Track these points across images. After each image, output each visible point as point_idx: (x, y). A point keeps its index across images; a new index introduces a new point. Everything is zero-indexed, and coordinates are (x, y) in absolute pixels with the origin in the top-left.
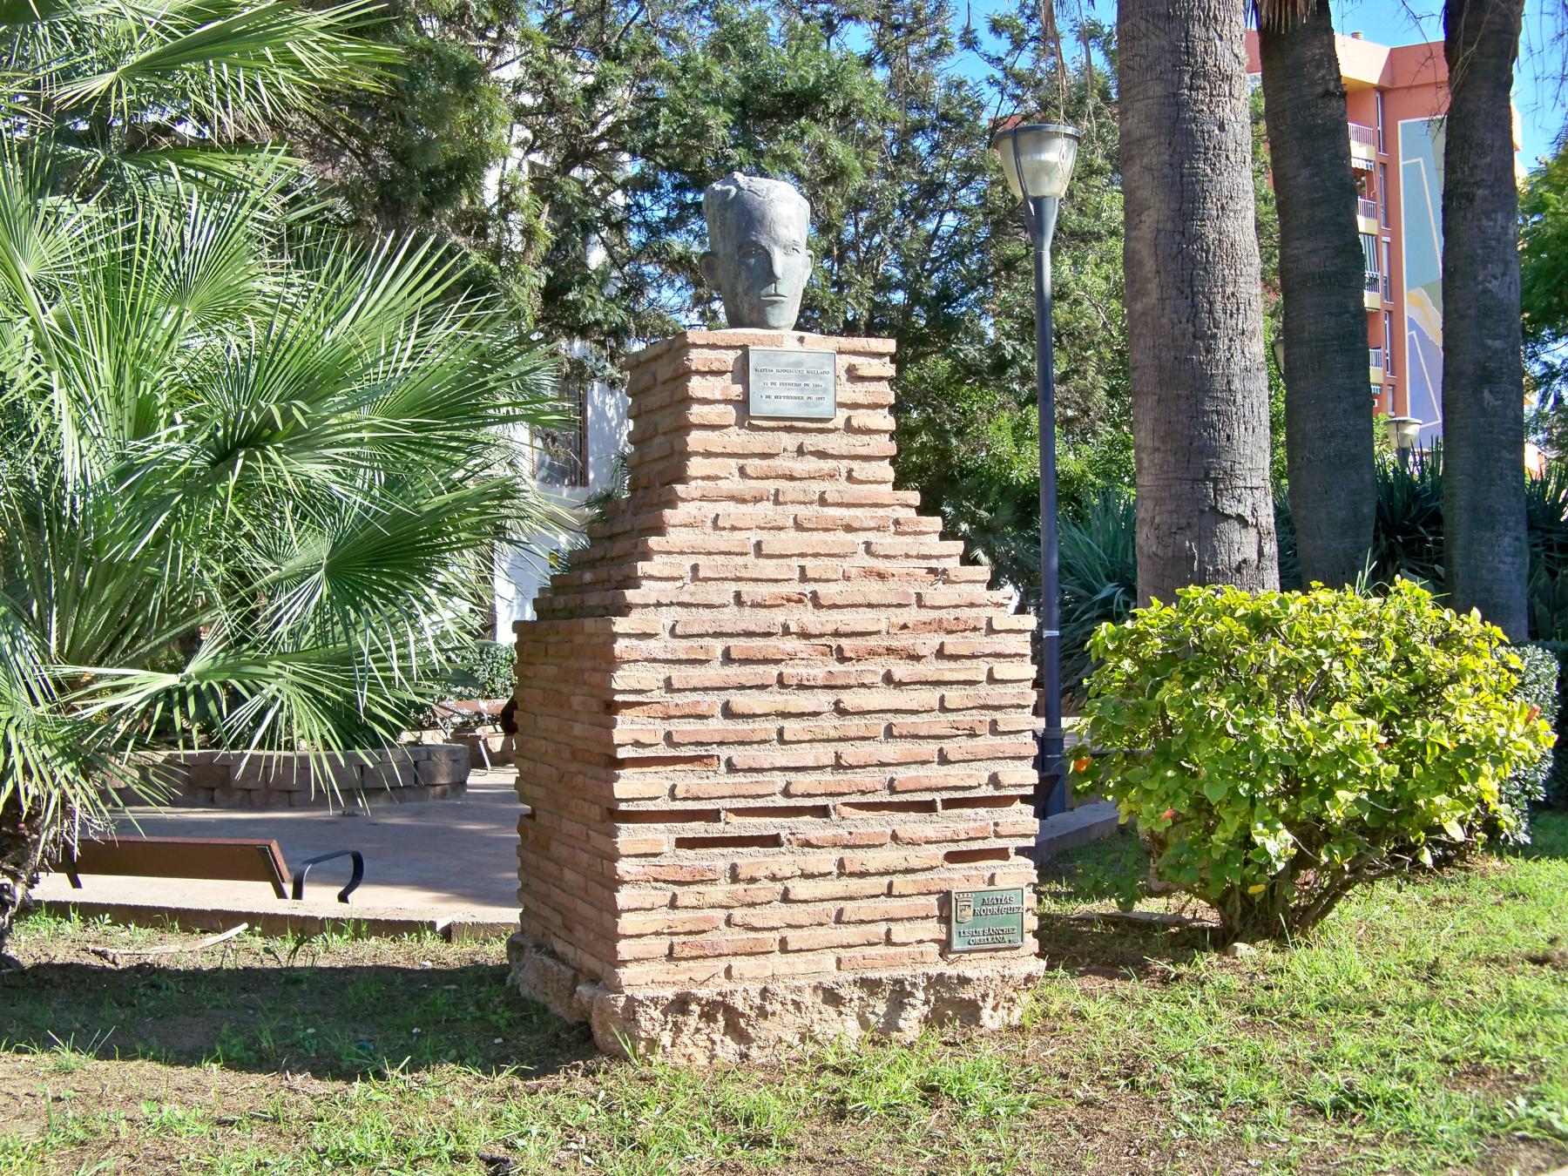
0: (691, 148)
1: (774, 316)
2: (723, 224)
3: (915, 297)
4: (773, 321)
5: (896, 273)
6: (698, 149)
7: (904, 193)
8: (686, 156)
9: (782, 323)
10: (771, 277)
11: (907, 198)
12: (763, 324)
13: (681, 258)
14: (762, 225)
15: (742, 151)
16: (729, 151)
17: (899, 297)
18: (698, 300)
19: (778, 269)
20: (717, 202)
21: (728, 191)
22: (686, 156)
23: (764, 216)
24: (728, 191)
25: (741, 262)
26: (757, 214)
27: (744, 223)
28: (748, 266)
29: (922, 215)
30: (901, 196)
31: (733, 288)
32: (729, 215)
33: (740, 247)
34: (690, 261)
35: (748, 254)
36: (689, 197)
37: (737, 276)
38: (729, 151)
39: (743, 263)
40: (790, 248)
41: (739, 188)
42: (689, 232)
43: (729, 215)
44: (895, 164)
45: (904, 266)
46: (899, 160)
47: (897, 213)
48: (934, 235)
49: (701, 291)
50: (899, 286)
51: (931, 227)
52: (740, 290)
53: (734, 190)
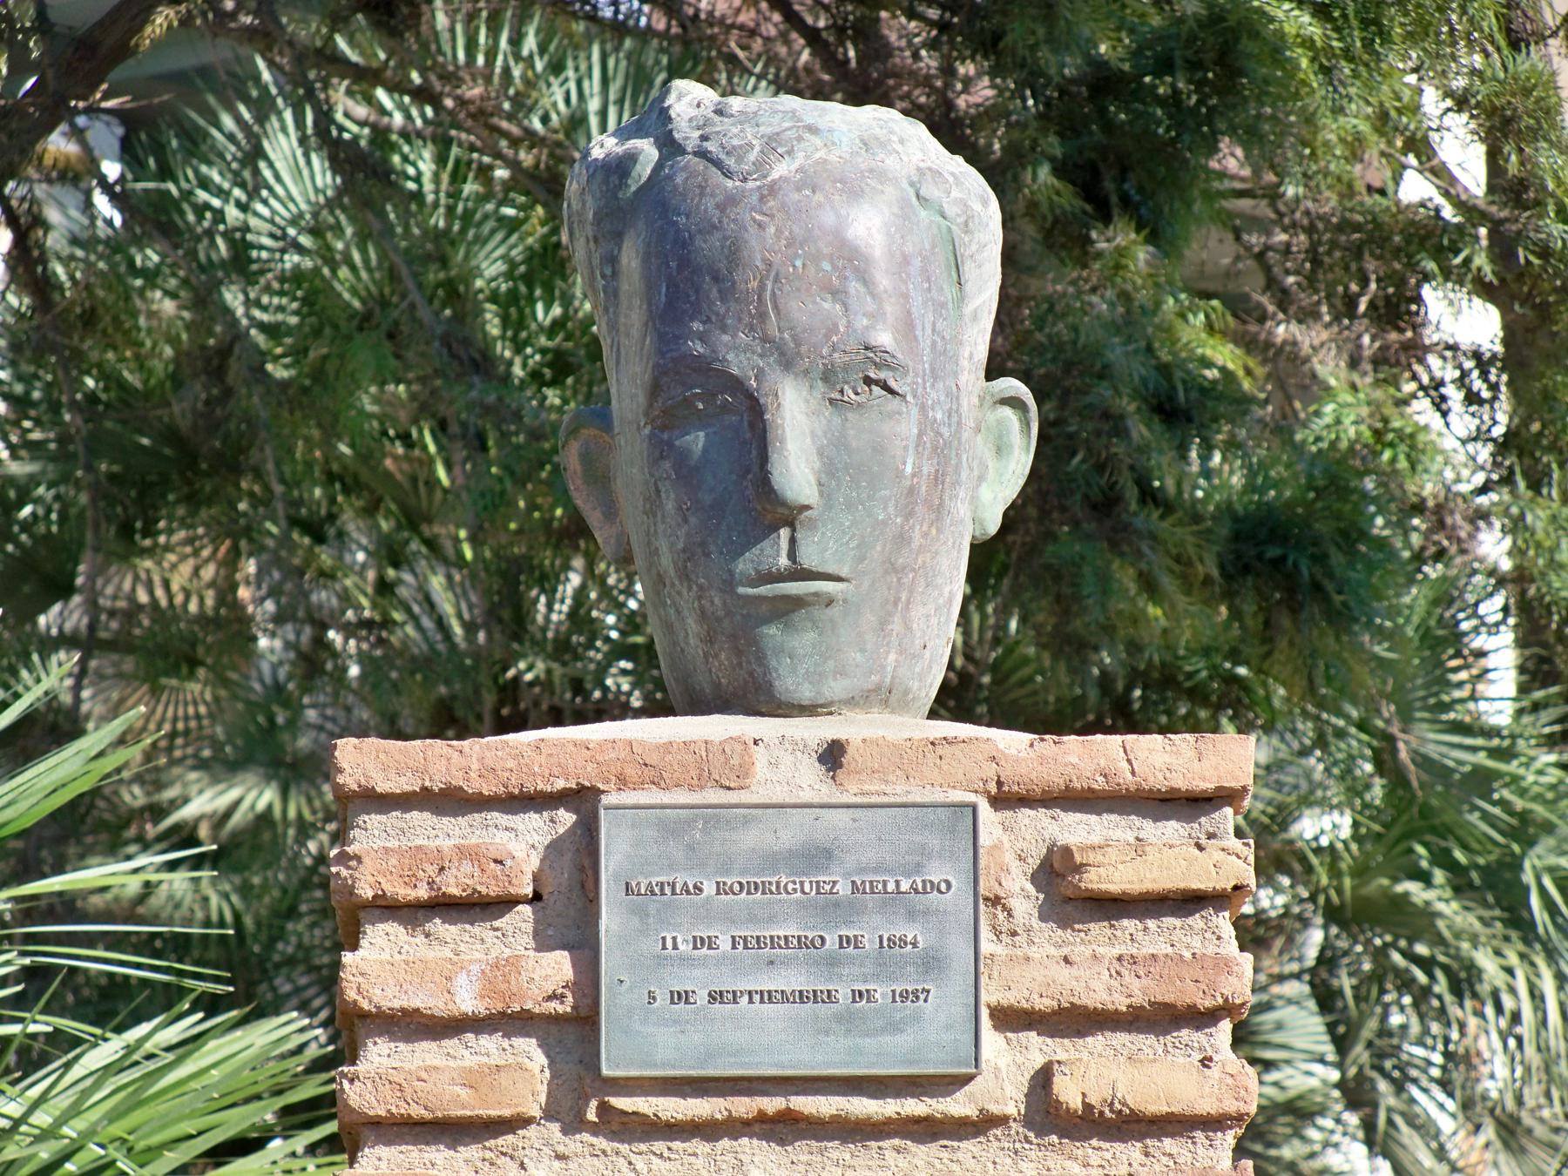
4: (791, 682)
9: (835, 688)
19: (797, 469)
23: (734, 253)
26: (708, 247)
28: (682, 457)
41: (670, 146)
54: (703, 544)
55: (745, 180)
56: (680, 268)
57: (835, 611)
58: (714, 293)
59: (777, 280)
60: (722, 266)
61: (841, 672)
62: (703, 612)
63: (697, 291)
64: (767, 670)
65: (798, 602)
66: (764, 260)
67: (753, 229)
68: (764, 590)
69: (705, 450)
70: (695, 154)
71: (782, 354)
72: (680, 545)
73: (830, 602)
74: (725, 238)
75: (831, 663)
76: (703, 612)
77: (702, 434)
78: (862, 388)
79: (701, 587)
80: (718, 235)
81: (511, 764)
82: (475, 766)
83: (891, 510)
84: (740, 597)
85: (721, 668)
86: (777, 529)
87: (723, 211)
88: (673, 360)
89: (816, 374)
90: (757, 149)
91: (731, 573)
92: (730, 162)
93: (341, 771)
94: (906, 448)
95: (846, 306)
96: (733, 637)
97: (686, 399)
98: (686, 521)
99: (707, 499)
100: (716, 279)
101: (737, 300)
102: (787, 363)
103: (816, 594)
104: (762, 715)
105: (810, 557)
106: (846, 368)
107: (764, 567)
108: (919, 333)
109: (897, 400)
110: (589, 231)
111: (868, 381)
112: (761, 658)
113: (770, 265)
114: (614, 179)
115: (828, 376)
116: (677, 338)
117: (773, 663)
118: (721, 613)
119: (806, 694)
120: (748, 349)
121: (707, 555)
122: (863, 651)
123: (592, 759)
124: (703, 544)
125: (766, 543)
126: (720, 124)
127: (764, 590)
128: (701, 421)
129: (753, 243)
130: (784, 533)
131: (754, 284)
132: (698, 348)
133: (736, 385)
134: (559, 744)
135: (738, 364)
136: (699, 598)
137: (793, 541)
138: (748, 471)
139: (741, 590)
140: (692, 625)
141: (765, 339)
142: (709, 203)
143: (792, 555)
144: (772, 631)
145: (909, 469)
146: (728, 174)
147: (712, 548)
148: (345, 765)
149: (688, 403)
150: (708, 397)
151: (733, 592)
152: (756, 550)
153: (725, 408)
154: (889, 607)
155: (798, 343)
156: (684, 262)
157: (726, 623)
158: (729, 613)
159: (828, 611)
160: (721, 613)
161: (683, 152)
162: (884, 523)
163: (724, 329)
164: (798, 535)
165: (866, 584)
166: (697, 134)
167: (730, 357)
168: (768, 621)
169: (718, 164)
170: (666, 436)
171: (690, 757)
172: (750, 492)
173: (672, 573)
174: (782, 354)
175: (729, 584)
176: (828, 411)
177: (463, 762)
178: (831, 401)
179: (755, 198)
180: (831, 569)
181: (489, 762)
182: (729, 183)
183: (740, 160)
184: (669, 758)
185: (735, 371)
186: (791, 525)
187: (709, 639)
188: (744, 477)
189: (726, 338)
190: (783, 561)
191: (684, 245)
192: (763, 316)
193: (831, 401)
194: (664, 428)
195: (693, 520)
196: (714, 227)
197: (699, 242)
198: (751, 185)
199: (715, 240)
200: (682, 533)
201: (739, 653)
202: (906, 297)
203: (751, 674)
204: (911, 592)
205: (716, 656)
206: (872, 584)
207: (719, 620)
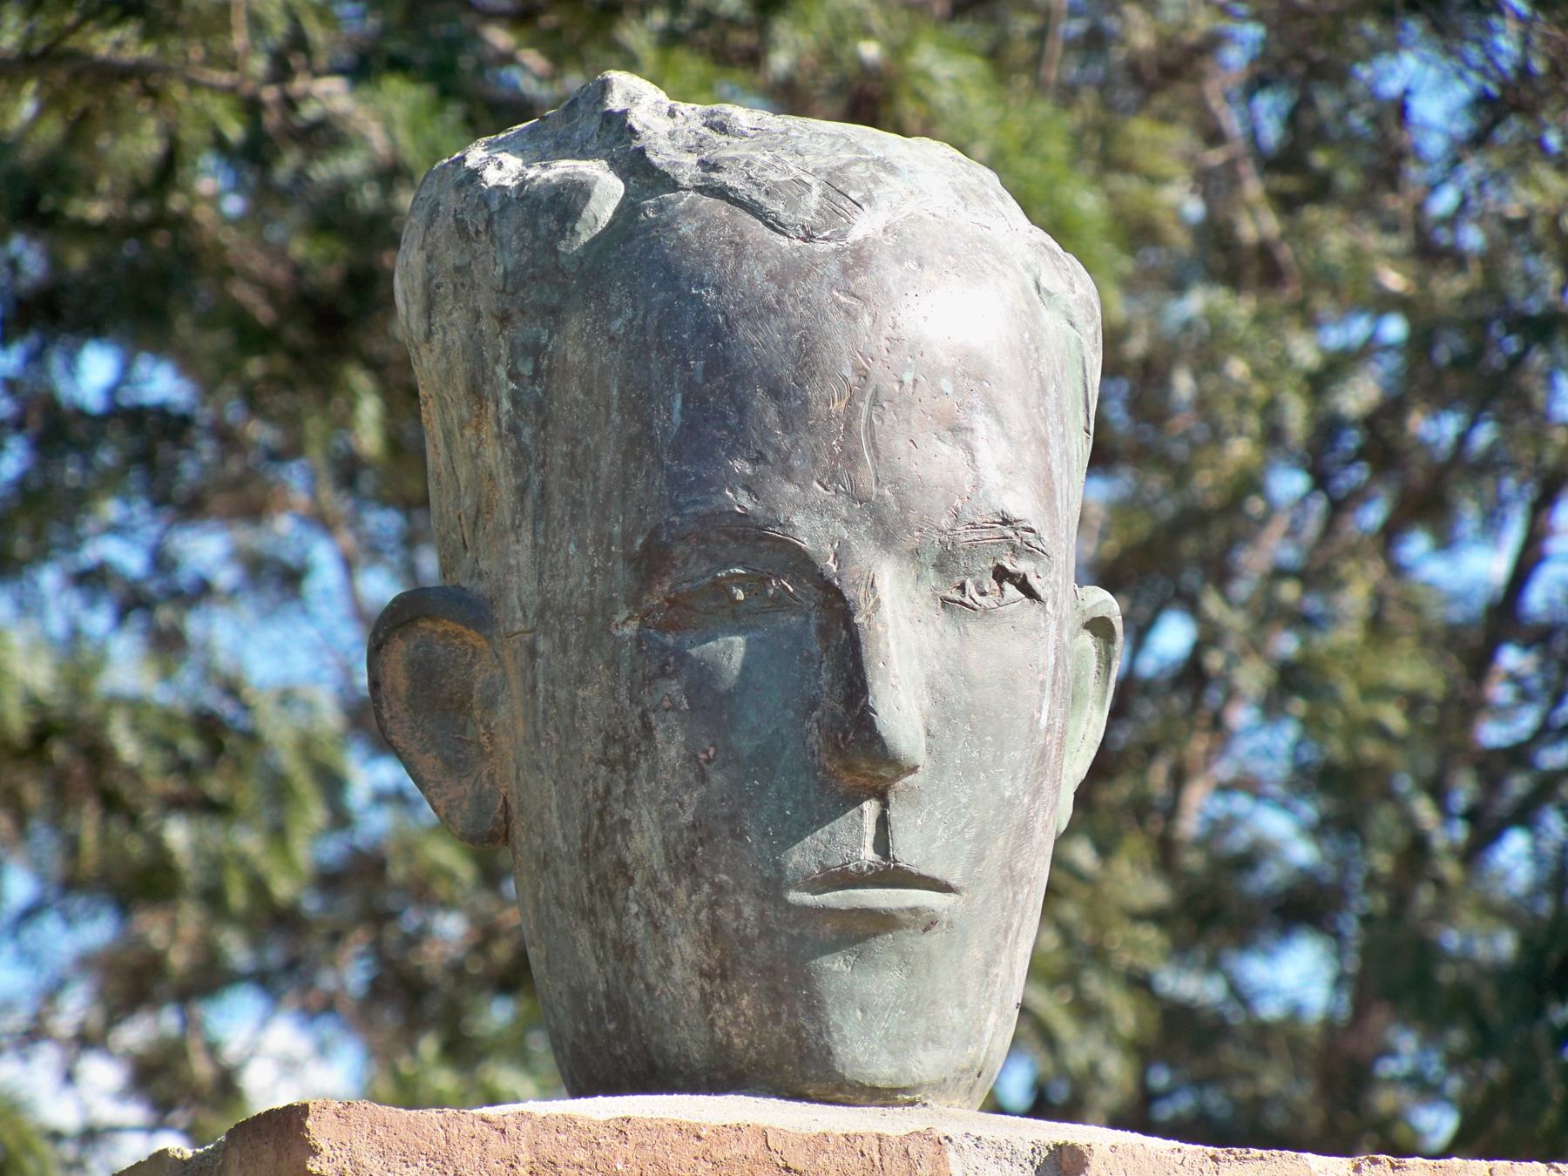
0: (111, 74)
1: (866, 1005)
2: (535, 409)
3: (1396, 973)
4: (860, 1049)
5: (1287, 837)
6: (147, 81)
7: (1336, 367)
8: (78, 130)
9: (925, 1064)
10: (852, 756)
11: (1358, 395)
12: (802, 1071)
13: (43, 732)
14: (795, 414)
15: (402, 96)
16: (329, 94)
17: (1296, 977)
18: (132, 983)
19: (901, 708)
20: (496, 264)
21: (566, 202)
22: (78, 130)
23: (806, 352)
24: (566, 202)
25: (659, 660)
26: (761, 342)
27: (694, 377)
28: (702, 679)
29: (1427, 504)
30: (1320, 382)
31: (602, 832)
32: (573, 343)
33: (650, 561)
34: (97, 753)
35: (706, 609)
36: (93, 373)
37: (626, 750)
38: (329, 94)
39: (672, 663)
40: (980, 568)
41: (638, 169)
42: (92, 580)
43: (573, 343)
44: (1286, 204)
45: (1341, 790)
46: (1295, 174)
47: (1289, 484)
48: (1505, 614)
49: (153, 928)
50: (1303, 908)
51: (1483, 565)
52: (645, 842)
53: (607, 190)
54: (732, 818)
55: (809, 238)
56: (709, 371)
57: (934, 939)
58: (771, 416)
59: (875, 401)
60: (786, 372)
61: (932, 1040)
62: (716, 927)
63: (741, 410)
64: (823, 1030)
65: (884, 921)
66: (857, 369)
67: (837, 319)
68: (833, 898)
69: (745, 668)
70: (699, 189)
71: (879, 521)
72: (687, 818)
73: (930, 924)
74: (790, 329)
75: (922, 1023)
76: (716, 927)
77: (739, 640)
78: (990, 584)
79: (719, 888)
80: (776, 323)
81: (580, 1156)
82: (525, 1157)
83: (1020, 783)
84: (790, 907)
85: (741, 1019)
86: (857, 802)
87: (782, 285)
88: (699, 518)
89: (928, 559)
90: (816, 191)
91: (779, 867)
92: (777, 207)
93: (314, 1152)
94: (1042, 689)
95: (969, 449)
96: (770, 971)
97: (716, 583)
98: (703, 778)
99: (746, 745)
100: (775, 393)
101: (810, 430)
102: (886, 537)
103: (915, 911)
104: (811, 1100)
105: (909, 851)
106: (973, 550)
107: (835, 862)
108: (1058, 503)
109: (1033, 608)
110: (485, 300)
111: (1001, 574)
112: (814, 1007)
113: (865, 376)
114: (547, 222)
115: (944, 562)
116: (703, 484)
117: (835, 1017)
118: (752, 931)
119: (882, 1070)
120: (824, 509)
121: (739, 836)
122: (962, 1005)
123: (706, 1156)
124: (732, 818)
125: (841, 823)
126: (726, 149)
127: (833, 898)
128: (736, 618)
129: (839, 339)
130: (870, 808)
131: (839, 406)
132: (743, 501)
133: (802, 564)
134: (655, 1128)
135: (809, 531)
136: (713, 905)
137: (883, 823)
138: (814, 705)
139: (794, 896)
140: (685, 948)
141: (856, 496)
142: (755, 272)
143: (882, 843)
144: (836, 966)
145: (1044, 722)
146: (776, 226)
147: (748, 825)
148: (322, 1143)
149: (720, 590)
150: (755, 583)
151: (779, 900)
152: (822, 834)
153: (781, 602)
154: (999, 938)
155: (905, 508)
156: (718, 364)
157: (760, 948)
158: (767, 933)
159: (924, 938)
160: (752, 931)
161: (675, 186)
162: (1010, 803)
163: (788, 474)
164: (893, 814)
165: (980, 899)
166: (691, 159)
167: (797, 520)
168: (832, 948)
169: (754, 209)
170: (670, 640)
171: (854, 1161)
172: (815, 739)
173: (657, 860)
174: (879, 521)
175: (773, 886)
176: (940, 618)
177: (507, 1149)
178: (945, 602)
179: (834, 268)
180: (936, 871)
181: (546, 1150)
182: (784, 242)
183: (792, 204)
184: (822, 1160)
185: (806, 545)
186: (882, 798)
187: (719, 974)
188: (807, 715)
189: (791, 489)
190: (868, 855)
191: (717, 334)
192: (852, 458)
193: (945, 602)
194: (665, 628)
195: (717, 778)
196: (770, 309)
197: (743, 330)
198: (820, 247)
199: (773, 330)
200: (692, 798)
201: (776, 997)
202: (1044, 443)
203: (795, 1032)
204: (1023, 916)
205: (730, 1000)
206: (986, 902)
207: (747, 943)
